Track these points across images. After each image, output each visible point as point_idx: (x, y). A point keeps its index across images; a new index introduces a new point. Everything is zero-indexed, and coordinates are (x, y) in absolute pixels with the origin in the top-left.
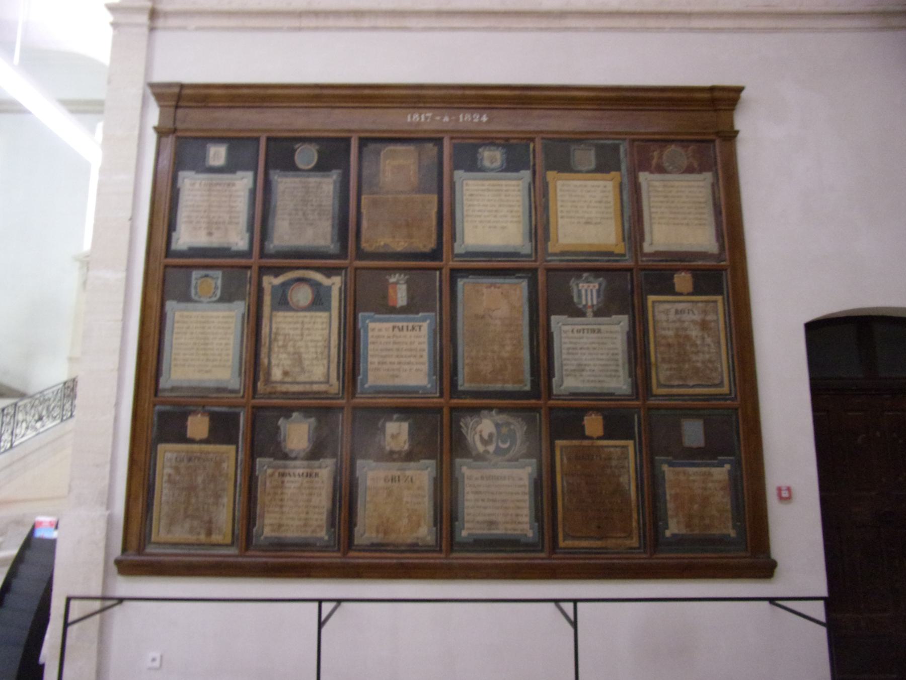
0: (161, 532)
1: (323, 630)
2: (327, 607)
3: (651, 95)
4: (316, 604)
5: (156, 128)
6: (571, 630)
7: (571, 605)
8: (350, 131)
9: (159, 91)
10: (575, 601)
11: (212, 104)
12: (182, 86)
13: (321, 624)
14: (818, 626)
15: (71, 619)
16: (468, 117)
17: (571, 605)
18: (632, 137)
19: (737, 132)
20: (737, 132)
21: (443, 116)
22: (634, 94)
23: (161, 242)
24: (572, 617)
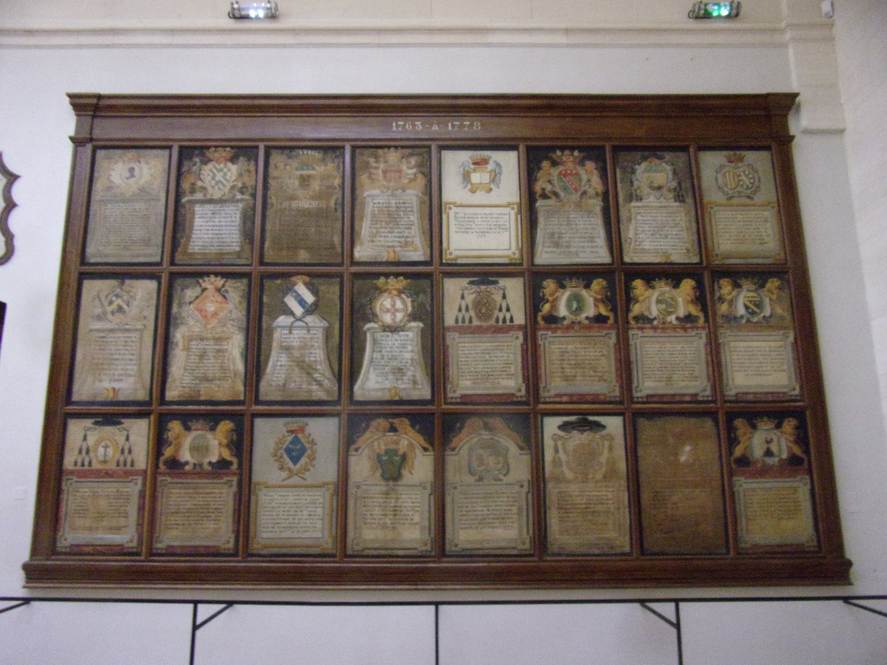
0: (71, 535)
3: (582, 102)
4: (191, 606)
5: (71, 139)
8: (172, 140)
10: (677, 601)
11: (103, 114)
12: (99, 97)
13: (195, 627)
14: (667, 626)
15: (199, 621)
18: (441, 143)
19: (793, 137)
20: (793, 137)
23: (75, 251)
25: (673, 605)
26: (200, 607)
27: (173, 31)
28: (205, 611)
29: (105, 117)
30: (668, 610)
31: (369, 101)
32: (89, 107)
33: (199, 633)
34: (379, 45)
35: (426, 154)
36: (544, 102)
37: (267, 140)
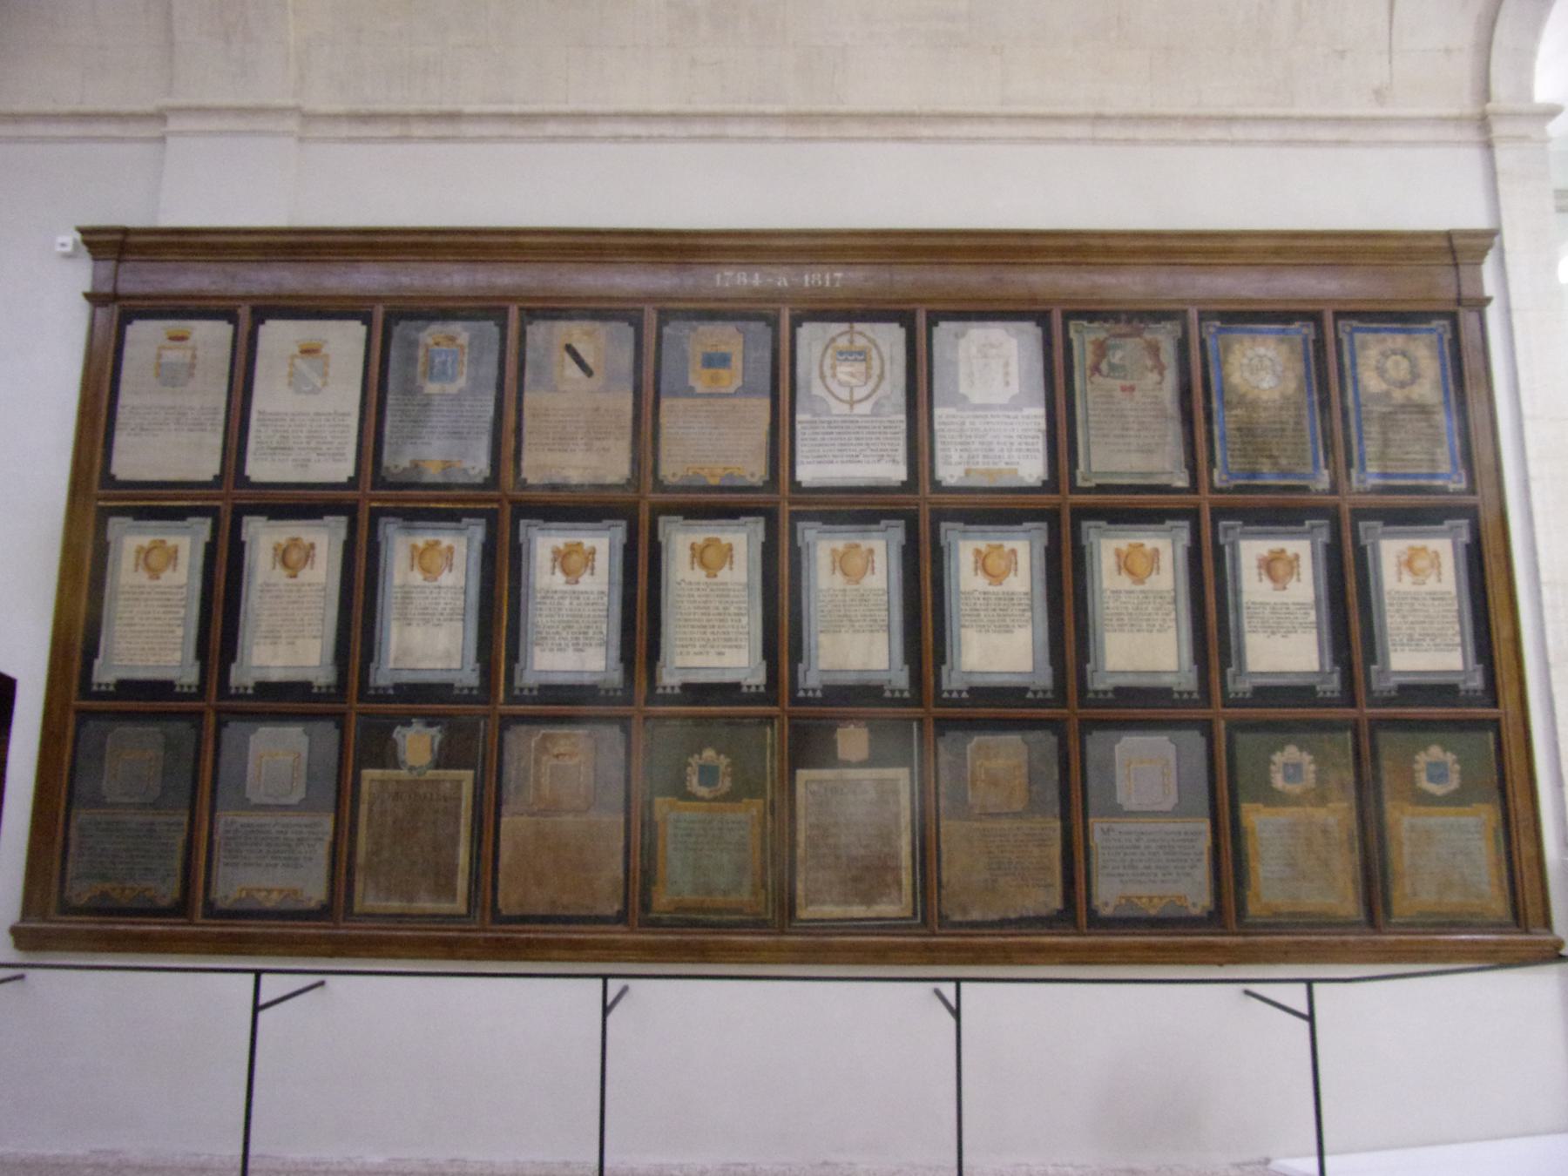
1: (610, 1019)
5: (87, 296)
6: (952, 1021)
7: (952, 986)
9: (89, 238)
11: (1094, 260)
12: (125, 231)
13: (606, 1010)
15: (263, 1000)
17: (952, 986)
21: (750, 276)
22: (305, 239)
24: (953, 1003)
26: (611, 982)
28: (614, 986)
29: (1095, 264)
31: (330, 238)
32: (108, 245)
33: (262, 1015)
35: (777, 322)
36: (1272, 243)
37: (930, 301)
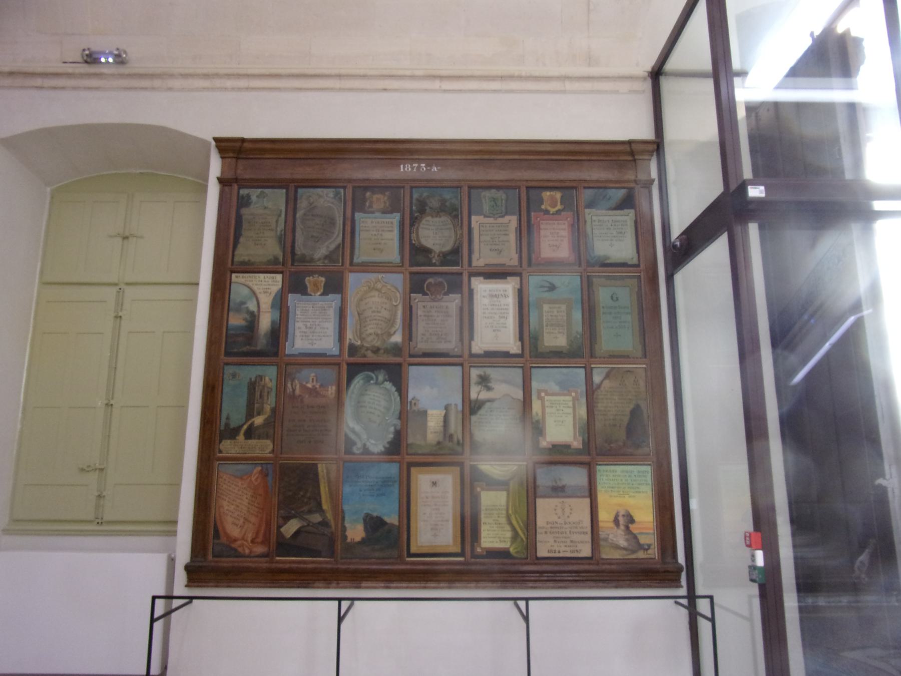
2: (345, 604)
3: (325, 145)
4: (337, 602)
5: (218, 178)
6: (525, 625)
10: (527, 599)
12: (243, 140)
13: (340, 619)
15: (156, 616)
16: (408, 168)
25: (337, 602)
27: (502, 78)
30: (522, 604)
32: (232, 149)
34: (592, 92)
